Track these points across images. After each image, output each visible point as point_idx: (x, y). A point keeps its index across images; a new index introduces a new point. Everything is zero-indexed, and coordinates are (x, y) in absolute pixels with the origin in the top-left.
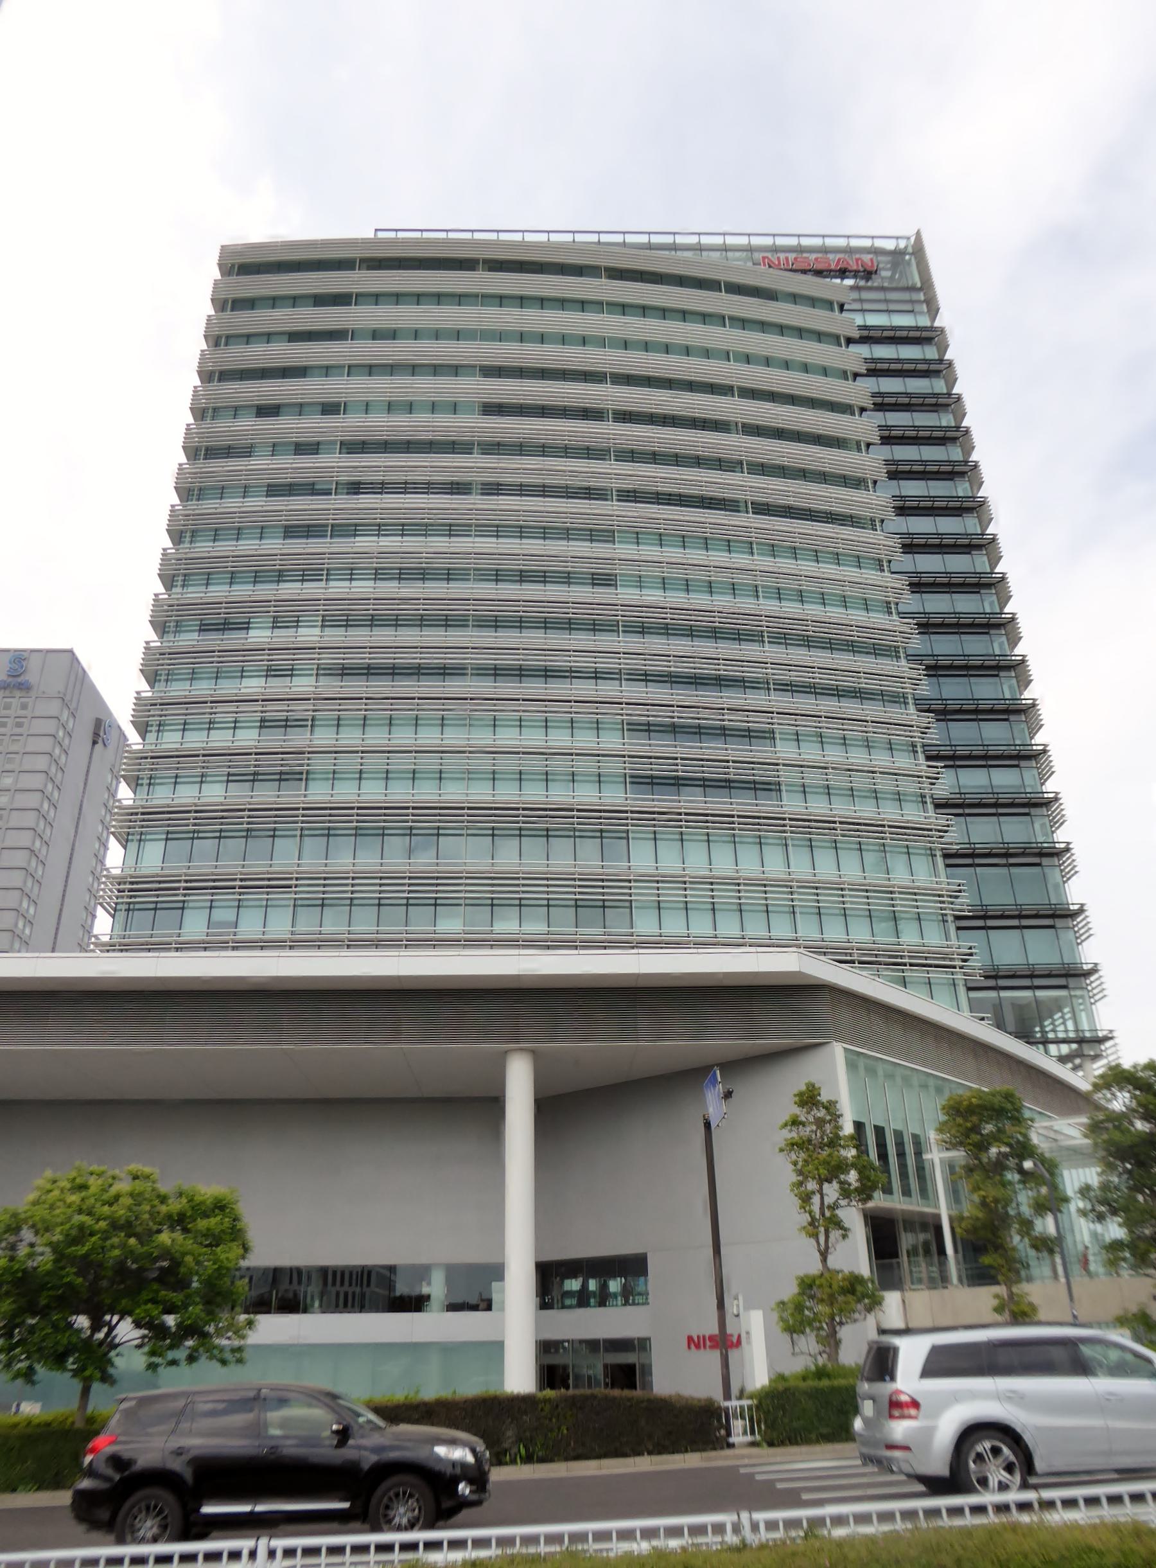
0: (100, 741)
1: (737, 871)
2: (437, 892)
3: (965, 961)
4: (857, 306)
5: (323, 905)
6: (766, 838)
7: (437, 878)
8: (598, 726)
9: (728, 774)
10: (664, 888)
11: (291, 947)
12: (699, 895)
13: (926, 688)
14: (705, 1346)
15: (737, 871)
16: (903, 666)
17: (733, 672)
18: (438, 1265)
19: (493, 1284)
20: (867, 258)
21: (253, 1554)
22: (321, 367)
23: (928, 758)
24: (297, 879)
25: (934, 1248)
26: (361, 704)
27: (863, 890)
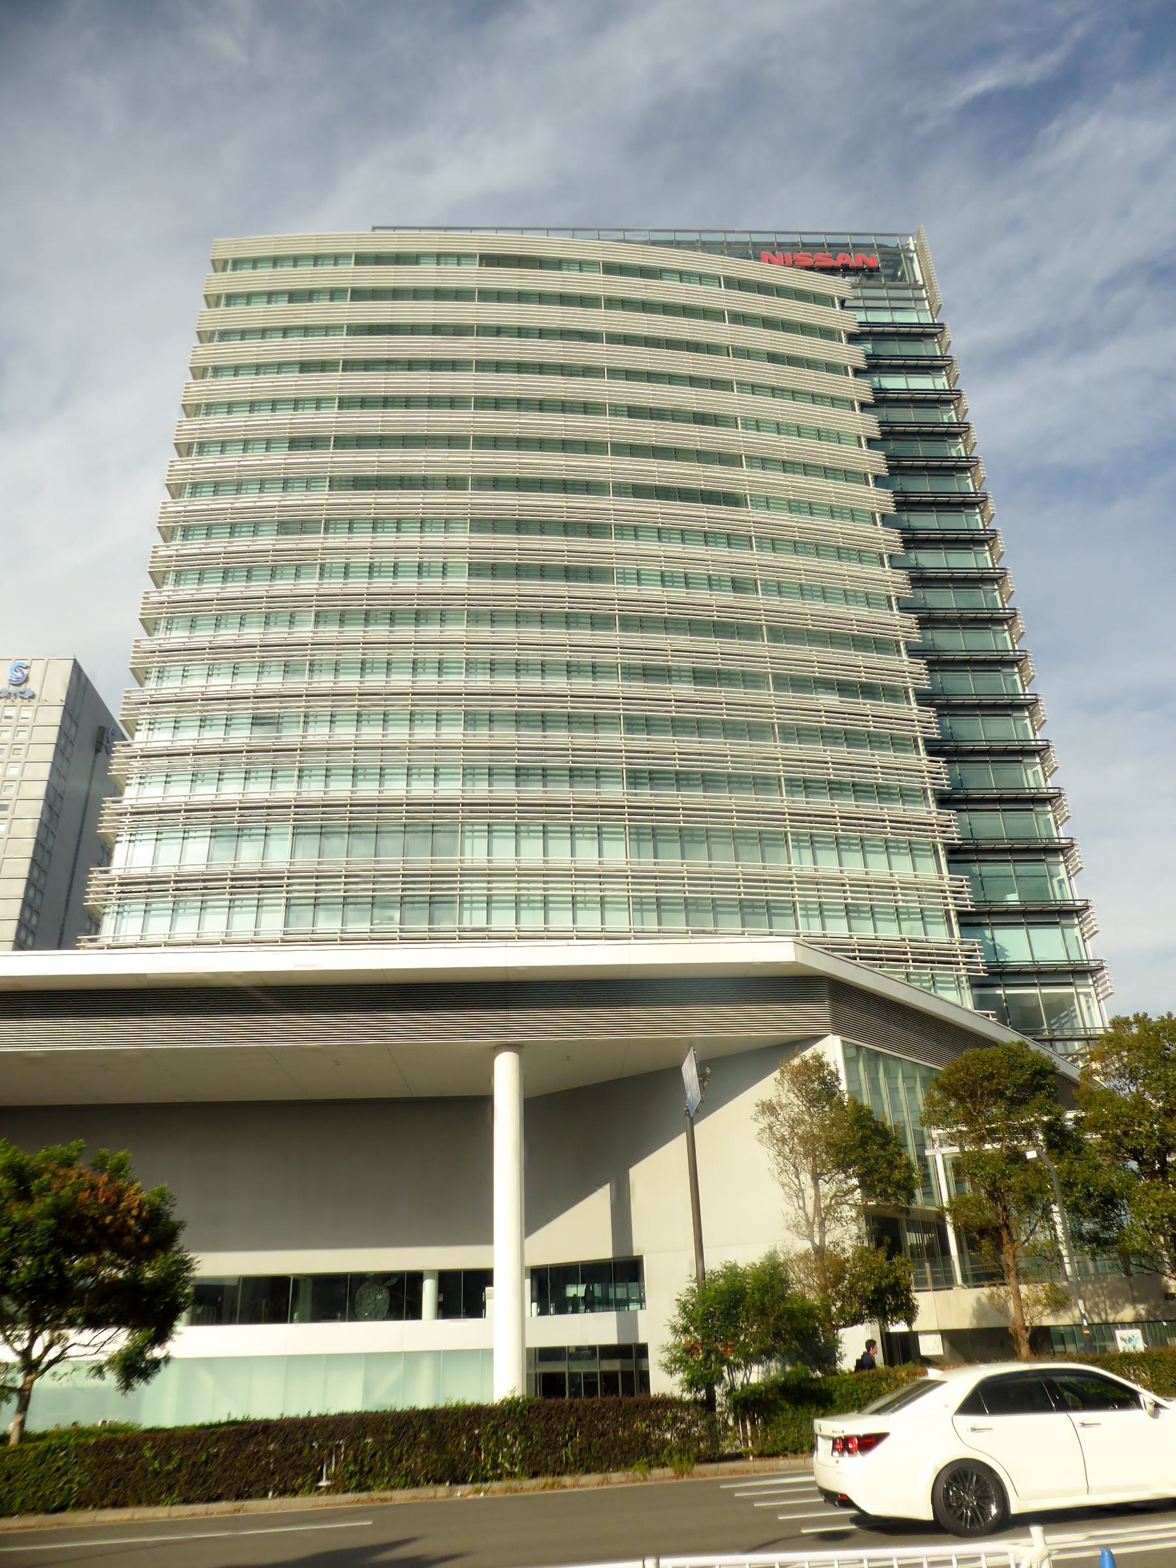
0: (103, 750)
3: (970, 957)
6: (868, 839)
12: (505, 888)
15: (841, 872)
17: (734, 666)
24: (289, 878)
25: (938, 1250)
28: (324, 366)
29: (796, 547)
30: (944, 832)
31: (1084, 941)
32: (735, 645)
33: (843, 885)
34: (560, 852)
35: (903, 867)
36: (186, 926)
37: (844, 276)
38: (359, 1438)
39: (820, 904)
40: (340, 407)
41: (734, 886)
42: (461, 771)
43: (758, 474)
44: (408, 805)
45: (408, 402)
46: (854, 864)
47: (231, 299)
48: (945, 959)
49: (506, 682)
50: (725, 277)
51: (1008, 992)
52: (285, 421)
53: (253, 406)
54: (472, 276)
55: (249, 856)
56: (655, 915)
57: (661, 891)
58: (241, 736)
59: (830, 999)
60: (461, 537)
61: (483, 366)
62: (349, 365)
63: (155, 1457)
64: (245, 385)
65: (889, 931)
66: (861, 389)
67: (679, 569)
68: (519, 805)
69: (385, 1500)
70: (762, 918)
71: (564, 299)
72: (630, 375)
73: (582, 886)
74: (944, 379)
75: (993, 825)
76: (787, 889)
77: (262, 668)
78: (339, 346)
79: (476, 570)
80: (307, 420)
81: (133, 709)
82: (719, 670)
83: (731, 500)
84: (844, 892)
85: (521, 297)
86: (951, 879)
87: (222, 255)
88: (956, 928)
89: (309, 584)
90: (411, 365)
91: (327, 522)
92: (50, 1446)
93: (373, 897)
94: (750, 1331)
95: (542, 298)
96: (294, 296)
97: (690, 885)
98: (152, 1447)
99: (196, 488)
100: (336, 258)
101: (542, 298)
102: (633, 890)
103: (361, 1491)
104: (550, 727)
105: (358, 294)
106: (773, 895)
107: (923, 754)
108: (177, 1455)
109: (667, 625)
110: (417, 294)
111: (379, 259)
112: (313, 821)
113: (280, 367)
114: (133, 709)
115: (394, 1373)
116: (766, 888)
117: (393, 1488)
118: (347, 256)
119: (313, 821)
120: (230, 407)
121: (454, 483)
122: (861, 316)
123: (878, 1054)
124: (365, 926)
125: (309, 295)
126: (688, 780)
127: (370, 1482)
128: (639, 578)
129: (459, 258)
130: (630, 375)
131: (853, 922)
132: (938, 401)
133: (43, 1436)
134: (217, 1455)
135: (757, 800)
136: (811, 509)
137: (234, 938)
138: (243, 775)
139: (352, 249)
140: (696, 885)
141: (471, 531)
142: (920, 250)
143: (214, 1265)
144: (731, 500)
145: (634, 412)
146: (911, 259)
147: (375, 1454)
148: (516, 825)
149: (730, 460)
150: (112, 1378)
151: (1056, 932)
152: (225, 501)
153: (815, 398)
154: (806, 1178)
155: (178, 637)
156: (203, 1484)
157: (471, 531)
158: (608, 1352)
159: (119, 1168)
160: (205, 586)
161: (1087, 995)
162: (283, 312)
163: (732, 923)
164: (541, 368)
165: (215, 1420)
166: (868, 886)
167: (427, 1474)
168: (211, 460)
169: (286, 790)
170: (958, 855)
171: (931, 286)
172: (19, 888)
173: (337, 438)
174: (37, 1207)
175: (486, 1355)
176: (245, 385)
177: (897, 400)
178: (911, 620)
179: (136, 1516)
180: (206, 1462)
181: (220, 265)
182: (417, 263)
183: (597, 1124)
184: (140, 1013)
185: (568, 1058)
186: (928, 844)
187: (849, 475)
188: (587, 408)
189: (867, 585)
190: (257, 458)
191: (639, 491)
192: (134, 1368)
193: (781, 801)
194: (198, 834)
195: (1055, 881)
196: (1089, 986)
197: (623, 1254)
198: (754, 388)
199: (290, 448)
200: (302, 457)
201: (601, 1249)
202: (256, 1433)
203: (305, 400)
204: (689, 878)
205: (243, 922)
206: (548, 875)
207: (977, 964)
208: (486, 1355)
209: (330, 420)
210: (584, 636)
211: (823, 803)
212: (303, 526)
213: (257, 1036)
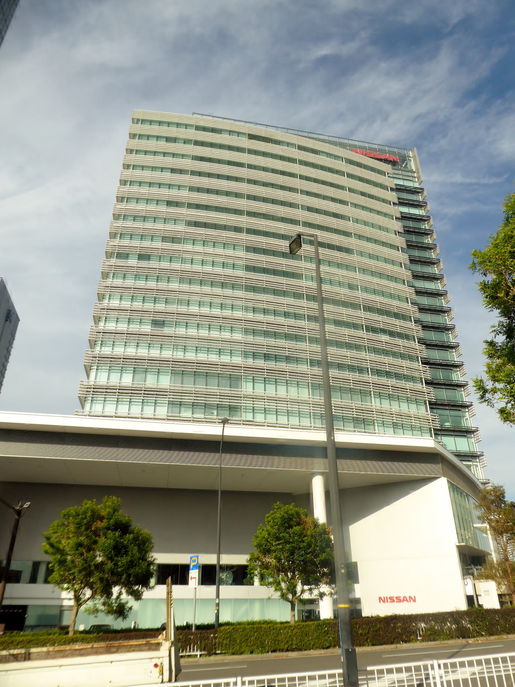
1: (298, 397)
2: (181, 399)
7: (182, 393)
8: (232, 330)
10: (279, 403)
13: (422, 334)
14: (387, 601)
16: (412, 325)
18: (43, 562)
21: (235, 684)
22: (139, 166)
23: (423, 363)
28: (181, 172)
33: (352, 409)
36: (123, 409)
42: (172, 347)
44: (172, 361)
45: (217, 192)
47: (141, 136)
49: (260, 317)
52: (165, 193)
54: (245, 143)
55: (151, 381)
57: (231, 402)
58: (147, 328)
60: (241, 253)
62: (193, 173)
64: (147, 175)
67: (231, 261)
70: (340, 422)
72: (308, 193)
73: (245, 402)
75: (444, 395)
77: (155, 300)
78: (188, 164)
80: (174, 194)
83: (348, 251)
85: (265, 154)
87: (136, 117)
89: (176, 266)
90: (219, 176)
92: (319, 624)
96: (168, 139)
99: (125, 217)
104: (256, 335)
105: (197, 143)
106: (346, 414)
110: (221, 146)
111: (204, 129)
112: (179, 370)
113: (162, 169)
115: (244, 607)
118: (192, 126)
121: (237, 230)
124: (202, 416)
125: (174, 140)
126: (269, 357)
128: (234, 266)
129: (239, 134)
132: (421, 219)
133: (228, 624)
137: (92, 414)
140: (222, 399)
143: (161, 558)
144: (348, 251)
151: (464, 440)
152: (139, 224)
153: (379, 213)
155: (118, 282)
160: (129, 260)
162: (162, 146)
163: (350, 426)
166: (401, 416)
168: (132, 205)
169: (167, 354)
170: (434, 405)
171: (418, 172)
176: (147, 175)
181: (135, 121)
184: (170, 449)
187: (392, 246)
189: (401, 293)
190: (152, 207)
195: (464, 418)
196: (477, 462)
198: (356, 206)
199: (167, 205)
203: (173, 185)
205: (149, 411)
209: (184, 195)
211: (384, 380)
212: (174, 240)
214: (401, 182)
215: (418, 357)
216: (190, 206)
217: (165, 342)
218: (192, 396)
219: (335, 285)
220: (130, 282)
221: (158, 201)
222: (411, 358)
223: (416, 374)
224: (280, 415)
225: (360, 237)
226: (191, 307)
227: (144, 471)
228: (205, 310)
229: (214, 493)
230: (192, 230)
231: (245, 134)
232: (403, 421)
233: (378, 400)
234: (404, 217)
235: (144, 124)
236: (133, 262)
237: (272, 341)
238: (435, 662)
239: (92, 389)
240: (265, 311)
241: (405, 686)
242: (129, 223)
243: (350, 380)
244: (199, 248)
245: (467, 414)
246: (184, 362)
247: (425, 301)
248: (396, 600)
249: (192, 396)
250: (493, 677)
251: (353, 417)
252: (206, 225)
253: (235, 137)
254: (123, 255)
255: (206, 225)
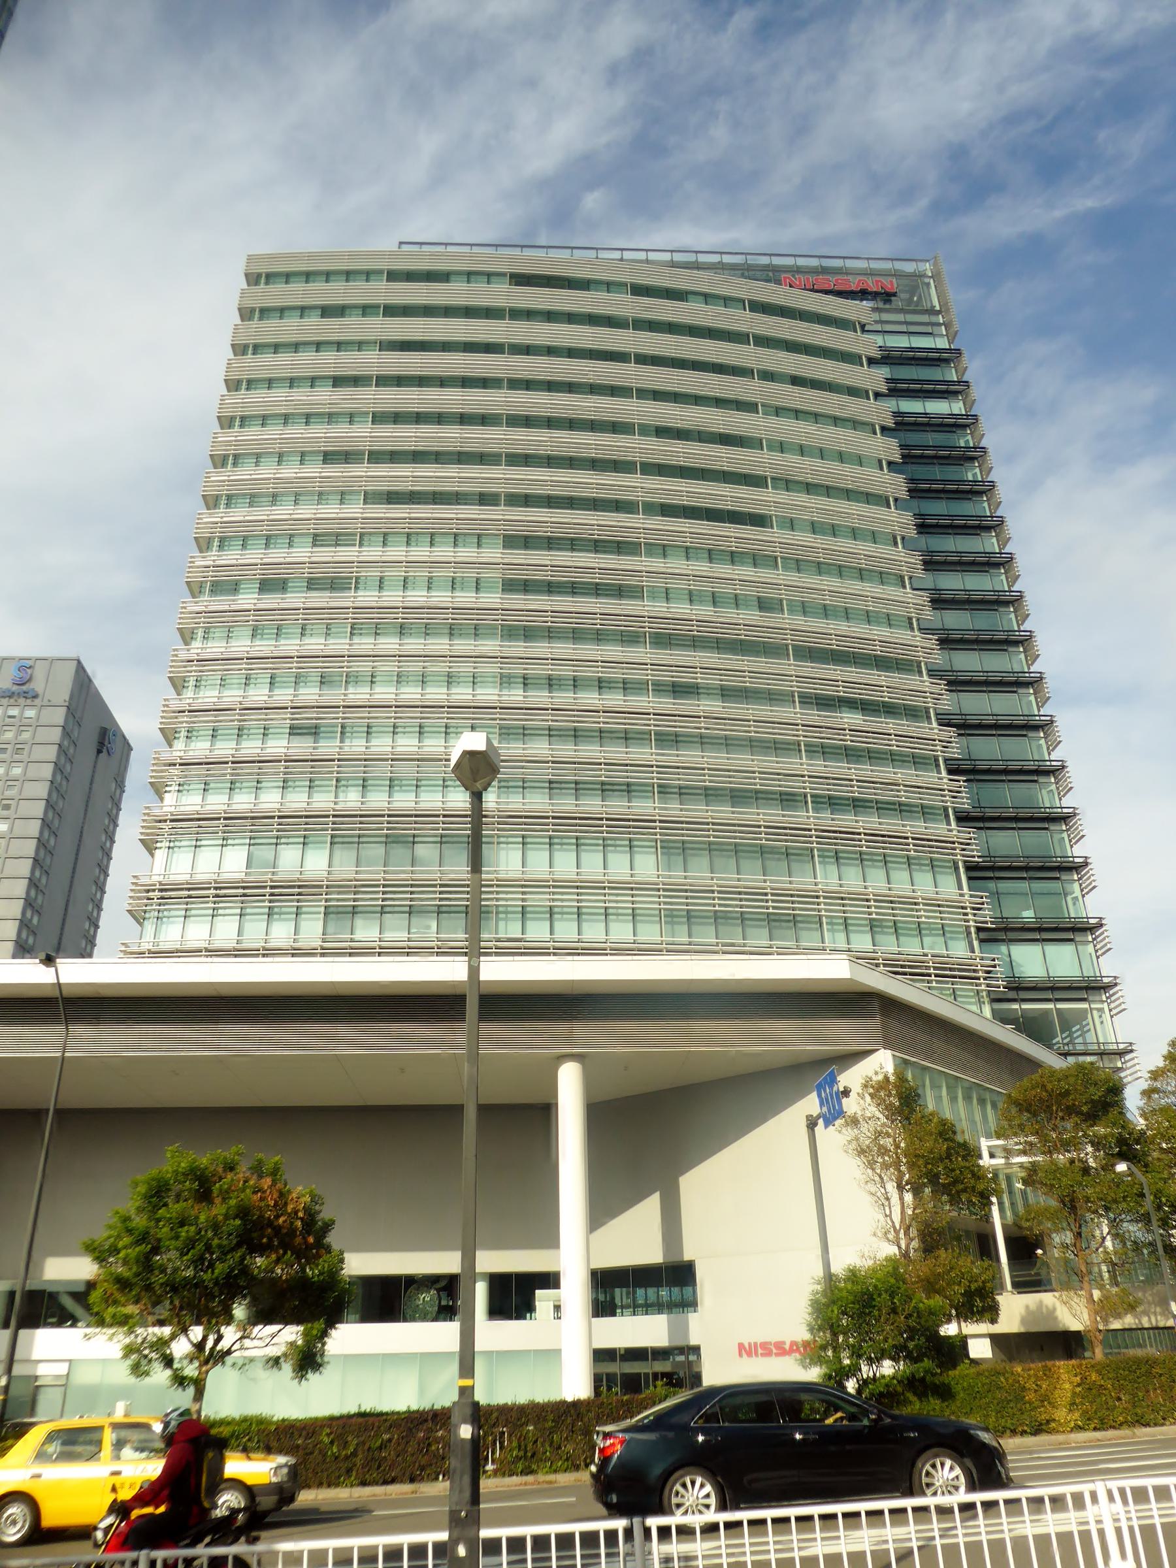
0: (105, 750)
3: (989, 972)
4: (878, 327)
5: (354, 913)
9: (755, 784)
11: (380, 954)
13: (948, 702)
14: (756, 1354)
16: (925, 682)
19: (539, 1293)
20: (886, 281)
23: (950, 772)
26: (390, 712)
27: (863, 900)
28: (356, 381)
29: (820, 568)
30: (964, 850)
31: (1098, 957)
32: (761, 663)
33: (817, 897)
34: (592, 865)
35: (925, 884)
37: (862, 300)
38: (522, 1425)
39: (846, 919)
40: (373, 422)
41: (762, 901)
43: (782, 496)
44: (389, 816)
46: (876, 882)
48: (965, 973)
49: (540, 697)
50: (749, 301)
51: (1024, 1006)
53: (286, 419)
56: (686, 927)
58: (278, 746)
59: (882, 1015)
60: (493, 553)
61: (516, 384)
62: (383, 381)
63: (332, 1443)
65: (912, 947)
66: (883, 411)
68: (554, 818)
69: (550, 1482)
71: (592, 320)
72: (658, 395)
74: (961, 404)
75: (1008, 843)
76: (813, 903)
77: (298, 680)
78: (372, 361)
79: (510, 586)
81: (171, 718)
82: (746, 688)
83: (759, 520)
84: (869, 907)
86: (971, 896)
88: (976, 943)
91: (362, 535)
92: (234, 1432)
93: (410, 906)
94: (887, 1333)
95: (571, 318)
96: (327, 311)
97: (773, 901)
98: (328, 1435)
100: (368, 275)
101: (571, 318)
102: (665, 903)
103: (527, 1474)
105: (391, 311)
107: (944, 774)
108: (353, 1442)
109: (695, 643)
110: (448, 311)
112: (343, 830)
113: (313, 381)
114: (171, 718)
116: (793, 902)
117: (555, 1471)
118: (379, 272)
119: (343, 830)
120: (264, 420)
121: (485, 499)
122: (879, 340)
123: (925, 1068)
125: (339, 311)
127: (534, 1467)
128: (668, 595)
130: (658, 395)
131: (877, 937)
134: (390, 1440)
135: (784, 816)
136: (834, 531)
138: (281, 784)
139: (385, 265)
141: (504, 547)
142: (936, 276)
143: (360, 1264)
144: (759, 520)
145: (662, 432)
146: (929, 284)
147: (536, 1442)
148: (550, 837)
149: (756, 481)
150: (287, 1368)
151: (1067, 950)
154: (891, 1187)
156: (379, 1467)
157: (504, 547)
158: (660, 1354)
159: (275, 1172)
161: (1101, 1010)
162: (315, 327)
163: (759, 937)
164: (570, 387)
165: (345, 1411)
166: (939, 906)
167: (585, 1460)
170: (978, 872)
171: (948, 310)
172: (20, 888)
173: (371, 453)
174: (219, 1209)
175: (553, 1355)
177: (915, 424)
178: (932, 642)
179: (320, 1497)
180: (380, 1448)
182: (448, 281)
183: (651, 1131)
185: (626, 1068)
186: (949, 861)
187: (869, 498)
188: (615, 427)
191: (667, 510)
192: (307, 1360)
193: (807, 817)
194: (237, 841)
195: (1069, 898)
197: (674, 1259)
199: (325, 462)
200: (334, 471)
201: (651, 1254)
202: (426, 1421)
204: (719, 892)
205: (281, 932)
206: (582, 887)
207: (997, 979)
208: (553, 1355)
209: (363, 434)
210: (613, 651)
211: (847, 820)
212: (338, 539)
213: (321, 1043)
214: (902, 342)
215: (936, 760)
216: (376, 457)
217: (319, 773)
218: (435, 892)
219: (724, 604)
220: (242, 644)
221: (303, 454)
222: (918, 761)
223: (934, 801)
224: (642, 921)
225: (787, 484)
226: (428, 690)
227: (402, 1070)
228: (411, 693)
229: (454, 1111)
230: (380, 511)
231: (503, 275)
232: (945, 919)
233: (833, 869)
234: (902, 425)
235: (274, 283)
236: (248, 599)
237: (616, 752)
238: (1100, 1487)
239: (268, 890)
240: (551, 683)
241: (722, 1565)
242: (239, 513)
243: (810, 830)
244: (396, 552)
245: (1076, 886)
246: (416, 816)
247: (957, 620)
248: (774, 1351)
249: (435, 892)
250: (1153, 1526)
251: (768, 914)
252: (413, 498)
253: (361, 284)
254: (226, 586)
255: (413, 498)
